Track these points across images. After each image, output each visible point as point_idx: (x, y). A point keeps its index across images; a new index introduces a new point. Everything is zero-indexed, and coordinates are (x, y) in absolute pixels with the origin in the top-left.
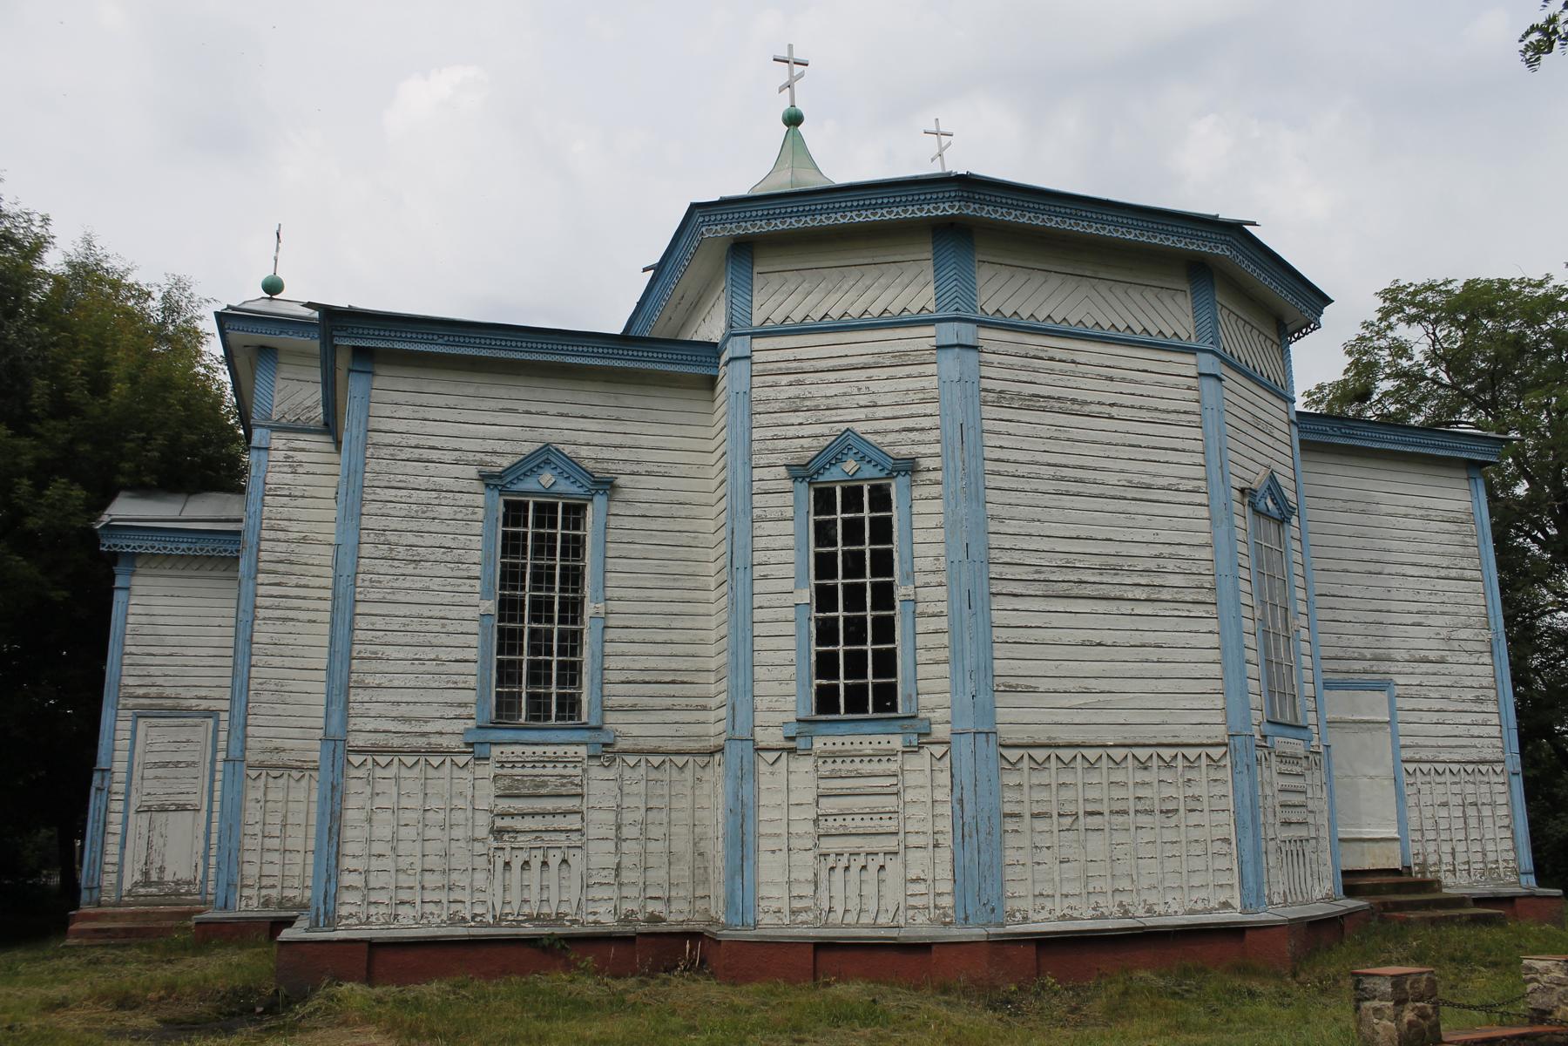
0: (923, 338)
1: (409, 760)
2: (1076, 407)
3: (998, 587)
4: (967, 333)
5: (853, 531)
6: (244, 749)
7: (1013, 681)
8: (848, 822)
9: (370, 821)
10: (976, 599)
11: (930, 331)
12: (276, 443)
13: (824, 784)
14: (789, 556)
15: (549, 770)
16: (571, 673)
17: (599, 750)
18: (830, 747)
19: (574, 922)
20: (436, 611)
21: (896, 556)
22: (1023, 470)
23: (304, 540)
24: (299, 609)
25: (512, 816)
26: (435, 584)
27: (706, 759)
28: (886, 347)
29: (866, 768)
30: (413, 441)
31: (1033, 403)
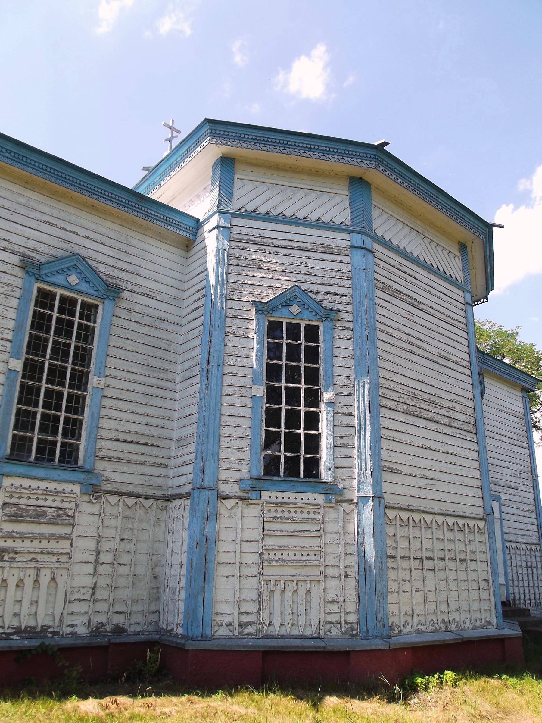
0: (341, 240)
2: (416, 303)
3: (384, 402)
4: (369, 243)
7: (391, 465)
11: (346, 236)
16: (73, 428)
19: (55, 633)
21: (321, 372)
22: (395, 333)
25: (14, 538)
27: (164, 503)
28: (320, 241)
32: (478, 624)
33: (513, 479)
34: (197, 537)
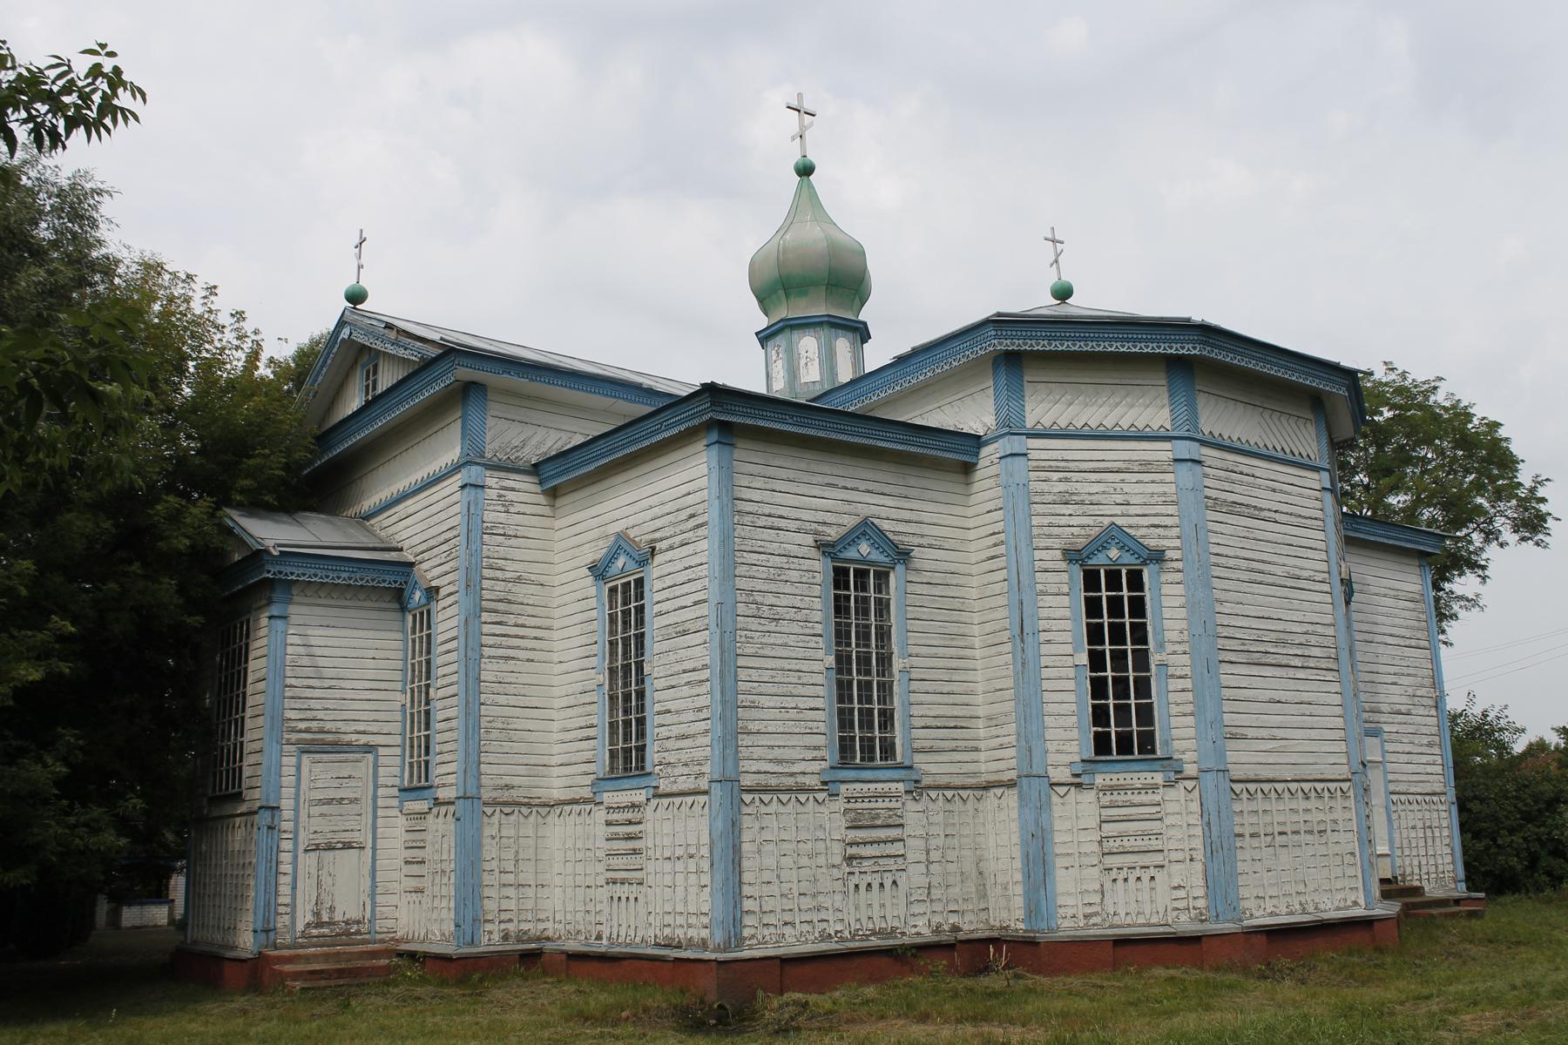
0: (1161, 452)
1: (784, 798)
5: (1115, 606)
6: (479, 786)
8: (1125, 843)
9: (759, 851)
10: (1208, 666)
11: (1167, 445)
12: (490, 482)
13: (1105, 812)
14: (1068, 625)
15: (880, 804)
17: (911, 786)
18: (1108, 782)
20: (794, 665)
21: (1149, 628)
22: (1231, 562)
23: (518, 580)
24: (518, 648)
25: (858, 844)
26: (791, 640)
29: (1137, 799)
30: (767, 509)
31: (1233, 508)
32: (1342, 904)
33: (1404, 700)
34: (1032, 828)
